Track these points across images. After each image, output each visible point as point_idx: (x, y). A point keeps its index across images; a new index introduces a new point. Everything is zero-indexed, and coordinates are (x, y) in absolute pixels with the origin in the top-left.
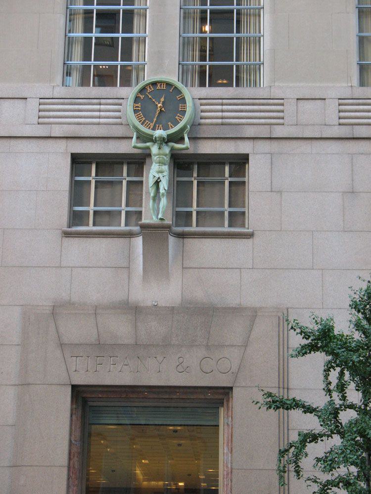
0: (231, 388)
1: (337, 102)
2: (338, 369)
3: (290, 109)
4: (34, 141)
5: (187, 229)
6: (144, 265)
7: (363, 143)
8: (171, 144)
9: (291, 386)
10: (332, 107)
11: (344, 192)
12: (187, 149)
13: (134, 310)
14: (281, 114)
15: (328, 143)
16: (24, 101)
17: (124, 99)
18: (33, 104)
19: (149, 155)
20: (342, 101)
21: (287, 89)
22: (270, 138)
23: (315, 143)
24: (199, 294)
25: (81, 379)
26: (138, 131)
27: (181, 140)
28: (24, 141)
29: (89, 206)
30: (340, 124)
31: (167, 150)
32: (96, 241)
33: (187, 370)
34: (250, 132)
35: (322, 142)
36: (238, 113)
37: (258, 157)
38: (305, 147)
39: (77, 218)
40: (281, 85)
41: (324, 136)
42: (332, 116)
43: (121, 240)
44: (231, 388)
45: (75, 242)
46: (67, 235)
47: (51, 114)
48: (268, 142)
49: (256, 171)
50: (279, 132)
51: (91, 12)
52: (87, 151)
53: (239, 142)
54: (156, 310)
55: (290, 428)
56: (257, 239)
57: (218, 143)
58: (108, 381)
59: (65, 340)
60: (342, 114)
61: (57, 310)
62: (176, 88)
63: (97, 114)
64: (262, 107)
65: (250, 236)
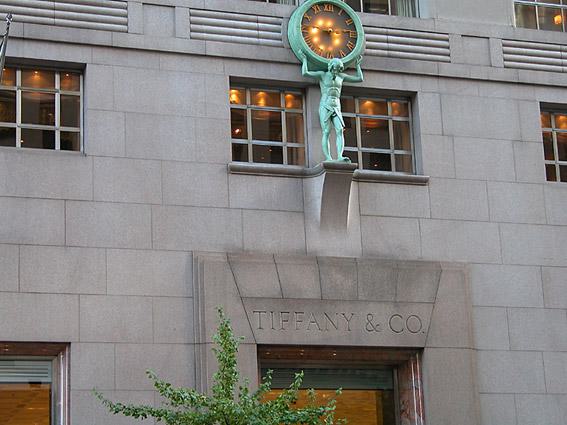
0: (421, 350)
1: (501, 42)
3: (456, 45)
4: (189, 58)
5: (386, 173)
6: (322, 209)
9: (480, 343)
10: (497, 47)
11: (514, 141)
13: (318, 261)
14: (447, 51)
15: (495, 86)
16: (171, 9)
19: (317, 86)
20: (507, 42)
21: (452, 23)
22: (438, 77)
24: (381, 246)
25: (266, 338)
26: (309, 59)
28: (176, 57)
29: (389, 155)
31: (339, 81)
32: (266, 179)
33: (376, 328)
34: (417, 67)
36: (229, 37)
37: (426, 95)
38: (472, 88)
39: (239, 152)
40: (444, 18)
41: (491, 79)
42: (498, 58)
44: (421, 350)
48: (435, 80)
49: (425, 107)
50: (446, 70)
52: (27, 56)
53: (408, 79)
54: (338, 263)
55: (21, 247)
56: (433, 186)
57: (34, 45)
58: (296, 340)
59: (245, 293)
61: (235, 258)
62: (344, 11)
63: (385, 37)
65: (423, 182)
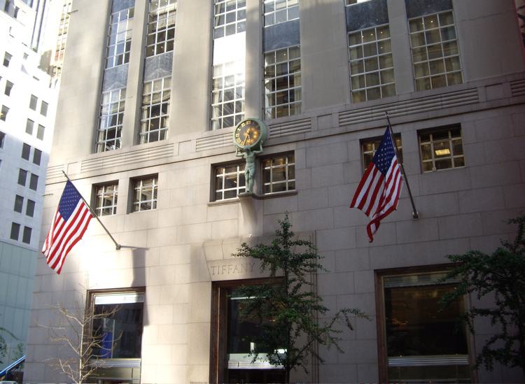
2: (499, 283)
7: (351, 134)
8: (255, 151)
12: (261, 153)
15: (333, 137)
17: (501, 84)
18: (194, 143)
22: (305, 140)
23: (327, 138)
27: (259, 149)
30: (340, 126)
31: (252, 154)
35: (330, 138)
38: (322, 142)
43: (235, 205)
45: (213, 208)
46: (209, 205)
47: (201, 146)
50: (309, 136)
51: (422, 34)
53: (290, 145)
60: (476, 97)
64: (300, 124)
